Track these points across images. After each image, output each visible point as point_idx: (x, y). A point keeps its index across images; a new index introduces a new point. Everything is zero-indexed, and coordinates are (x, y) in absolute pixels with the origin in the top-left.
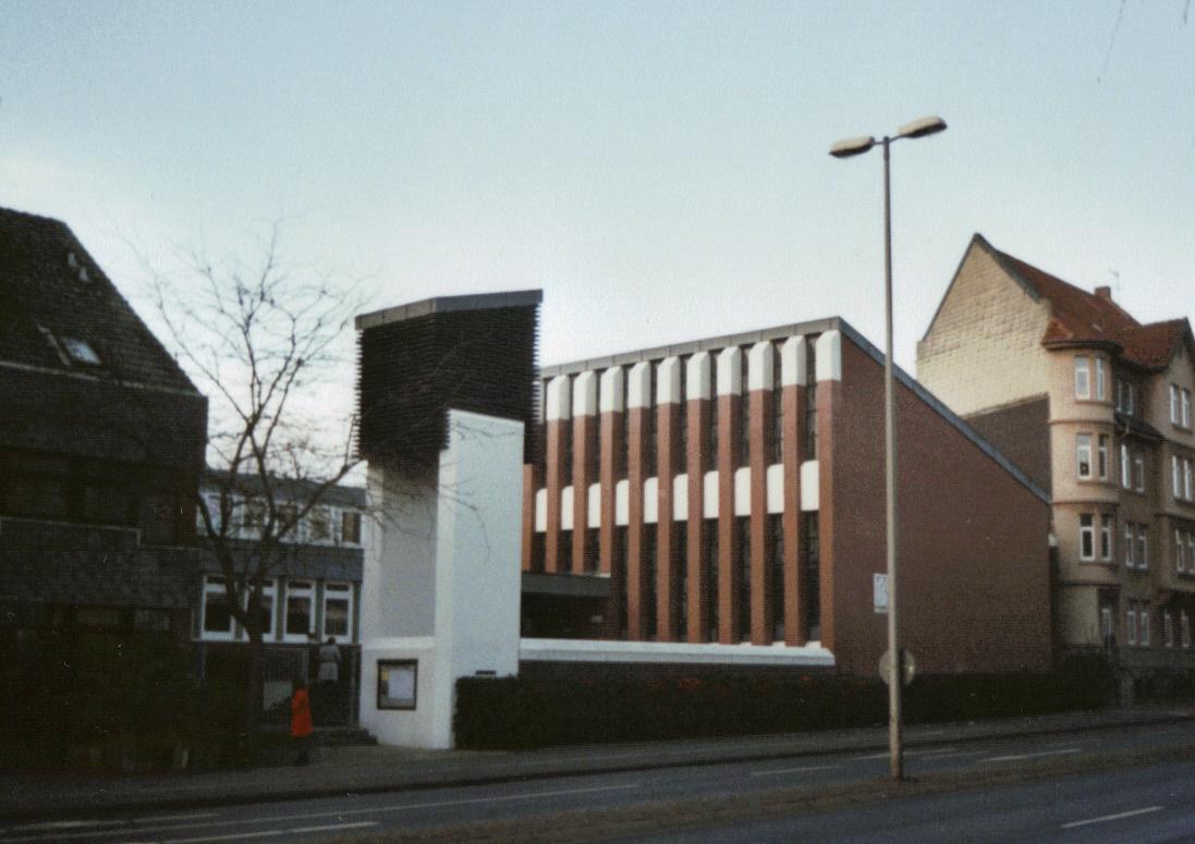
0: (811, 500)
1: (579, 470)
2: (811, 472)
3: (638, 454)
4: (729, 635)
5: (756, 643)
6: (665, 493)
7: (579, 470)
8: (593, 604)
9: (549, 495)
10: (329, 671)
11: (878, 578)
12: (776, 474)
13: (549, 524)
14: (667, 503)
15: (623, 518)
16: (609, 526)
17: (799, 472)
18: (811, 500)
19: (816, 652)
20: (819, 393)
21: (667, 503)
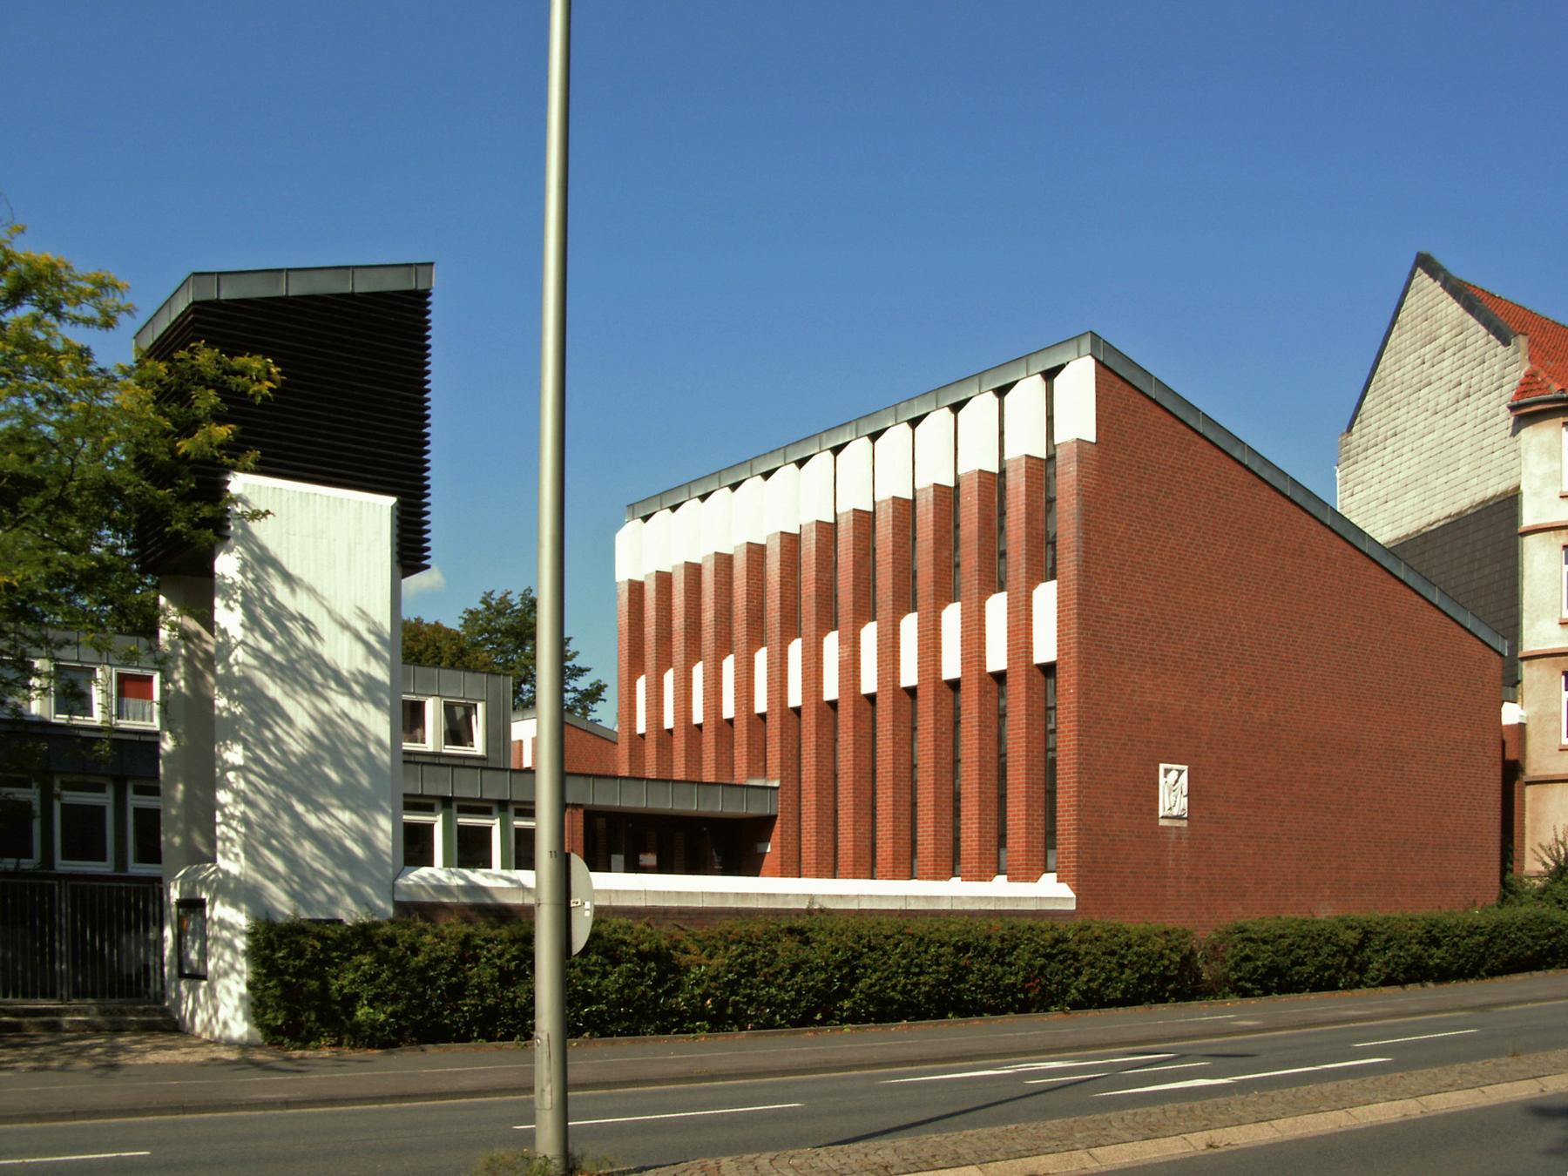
0: (1045, 649)
1: (740, 630)
2: (1046, 597)
3: (813, 594)
4: (930, 868)
5: (966, 879)
6: (847, 651)
7: (740, 630)
8: (761, 827)
9: (737, 662)
10: (259, 373)
11: (1167, 771)
12: (997, 607)
13: (966, 661)
14: (851, 667)
15: (869, 683)
16: (777, 710)
17: (1029, 598)
18: (1045, 649)
19: (1051, 891)
20: (1010, 475)
21: (851, 667)
